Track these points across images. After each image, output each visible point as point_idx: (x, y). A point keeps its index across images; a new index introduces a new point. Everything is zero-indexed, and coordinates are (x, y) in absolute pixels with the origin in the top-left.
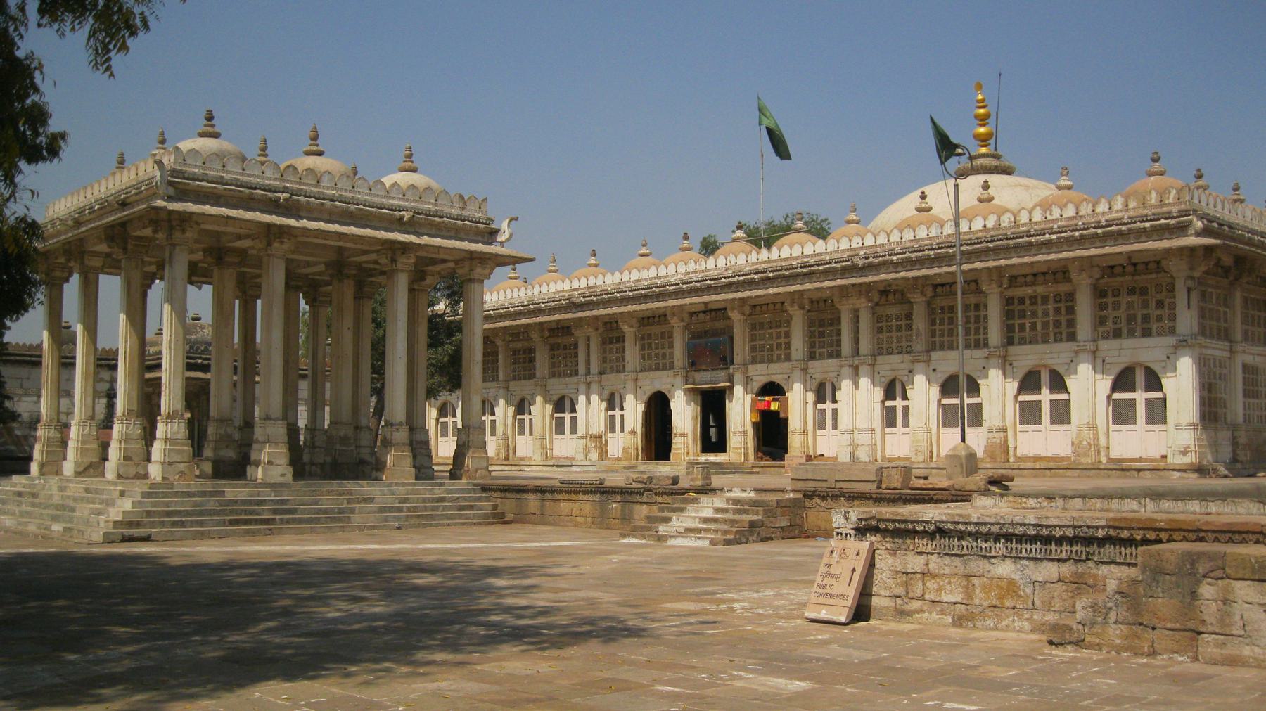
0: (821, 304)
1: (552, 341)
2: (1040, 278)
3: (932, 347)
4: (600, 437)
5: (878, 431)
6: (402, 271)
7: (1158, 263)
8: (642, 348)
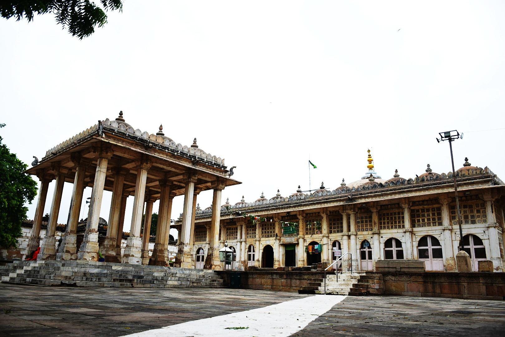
0: (334, 213)
1: (227, 227)
2: (425, 203)
3: (380, 228)
4: (245, 262)
5: (359, 260)
6: (192, 182)
7: (398, 204)
8: (263, 229)
